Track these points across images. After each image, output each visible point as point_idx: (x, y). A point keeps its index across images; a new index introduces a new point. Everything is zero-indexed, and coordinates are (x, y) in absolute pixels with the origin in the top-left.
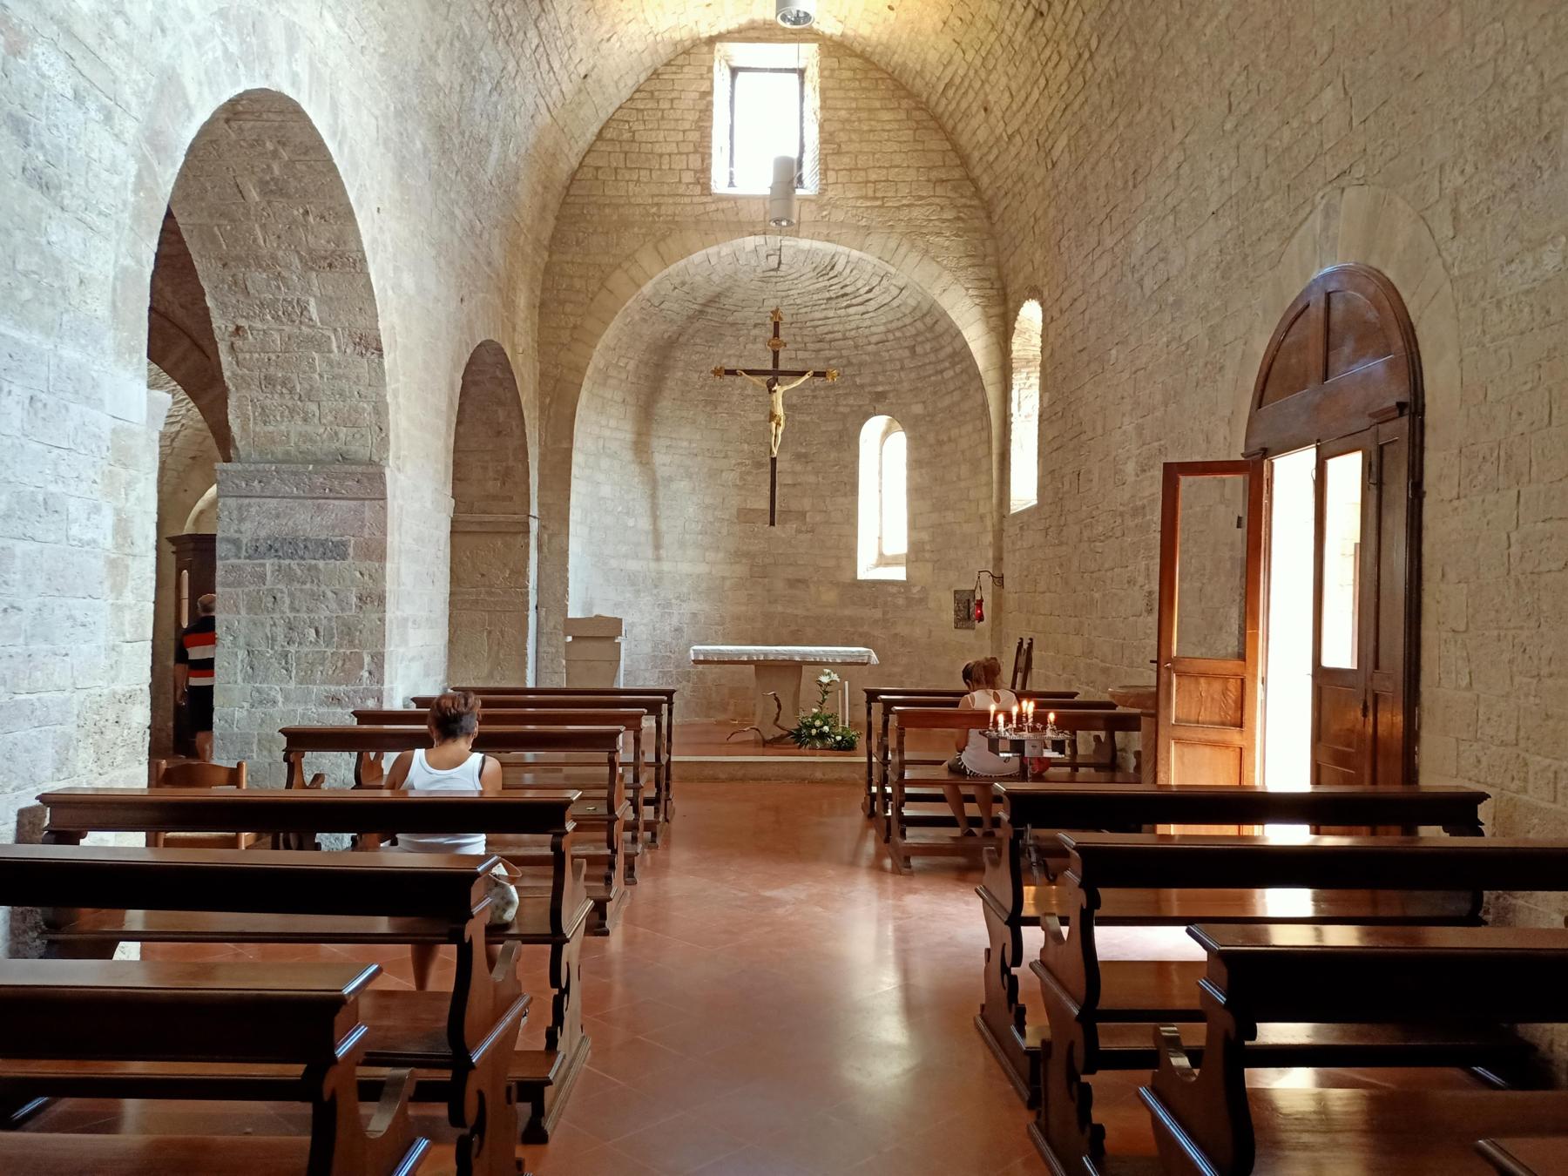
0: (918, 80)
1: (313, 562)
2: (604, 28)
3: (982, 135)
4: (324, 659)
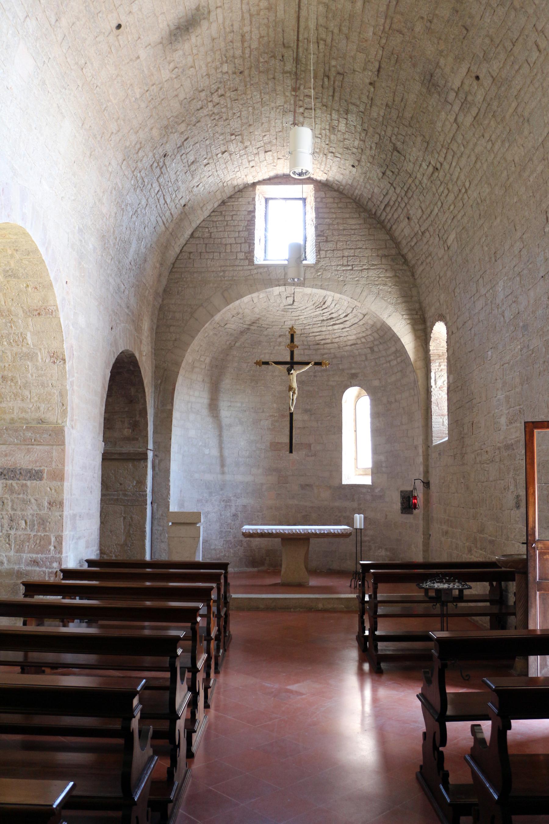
0: (370, 203)
1: (24, 482)
2: (195, 180)
3: (407, 232)
4: (29, 539)
